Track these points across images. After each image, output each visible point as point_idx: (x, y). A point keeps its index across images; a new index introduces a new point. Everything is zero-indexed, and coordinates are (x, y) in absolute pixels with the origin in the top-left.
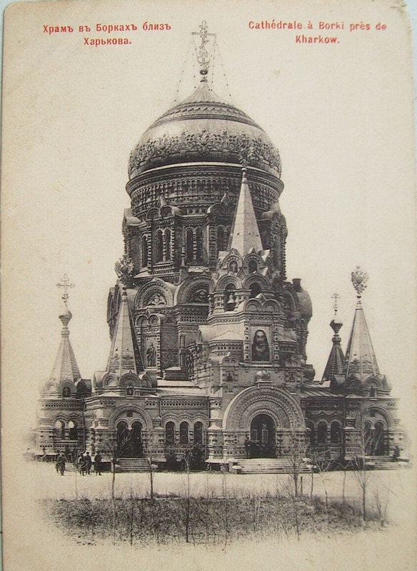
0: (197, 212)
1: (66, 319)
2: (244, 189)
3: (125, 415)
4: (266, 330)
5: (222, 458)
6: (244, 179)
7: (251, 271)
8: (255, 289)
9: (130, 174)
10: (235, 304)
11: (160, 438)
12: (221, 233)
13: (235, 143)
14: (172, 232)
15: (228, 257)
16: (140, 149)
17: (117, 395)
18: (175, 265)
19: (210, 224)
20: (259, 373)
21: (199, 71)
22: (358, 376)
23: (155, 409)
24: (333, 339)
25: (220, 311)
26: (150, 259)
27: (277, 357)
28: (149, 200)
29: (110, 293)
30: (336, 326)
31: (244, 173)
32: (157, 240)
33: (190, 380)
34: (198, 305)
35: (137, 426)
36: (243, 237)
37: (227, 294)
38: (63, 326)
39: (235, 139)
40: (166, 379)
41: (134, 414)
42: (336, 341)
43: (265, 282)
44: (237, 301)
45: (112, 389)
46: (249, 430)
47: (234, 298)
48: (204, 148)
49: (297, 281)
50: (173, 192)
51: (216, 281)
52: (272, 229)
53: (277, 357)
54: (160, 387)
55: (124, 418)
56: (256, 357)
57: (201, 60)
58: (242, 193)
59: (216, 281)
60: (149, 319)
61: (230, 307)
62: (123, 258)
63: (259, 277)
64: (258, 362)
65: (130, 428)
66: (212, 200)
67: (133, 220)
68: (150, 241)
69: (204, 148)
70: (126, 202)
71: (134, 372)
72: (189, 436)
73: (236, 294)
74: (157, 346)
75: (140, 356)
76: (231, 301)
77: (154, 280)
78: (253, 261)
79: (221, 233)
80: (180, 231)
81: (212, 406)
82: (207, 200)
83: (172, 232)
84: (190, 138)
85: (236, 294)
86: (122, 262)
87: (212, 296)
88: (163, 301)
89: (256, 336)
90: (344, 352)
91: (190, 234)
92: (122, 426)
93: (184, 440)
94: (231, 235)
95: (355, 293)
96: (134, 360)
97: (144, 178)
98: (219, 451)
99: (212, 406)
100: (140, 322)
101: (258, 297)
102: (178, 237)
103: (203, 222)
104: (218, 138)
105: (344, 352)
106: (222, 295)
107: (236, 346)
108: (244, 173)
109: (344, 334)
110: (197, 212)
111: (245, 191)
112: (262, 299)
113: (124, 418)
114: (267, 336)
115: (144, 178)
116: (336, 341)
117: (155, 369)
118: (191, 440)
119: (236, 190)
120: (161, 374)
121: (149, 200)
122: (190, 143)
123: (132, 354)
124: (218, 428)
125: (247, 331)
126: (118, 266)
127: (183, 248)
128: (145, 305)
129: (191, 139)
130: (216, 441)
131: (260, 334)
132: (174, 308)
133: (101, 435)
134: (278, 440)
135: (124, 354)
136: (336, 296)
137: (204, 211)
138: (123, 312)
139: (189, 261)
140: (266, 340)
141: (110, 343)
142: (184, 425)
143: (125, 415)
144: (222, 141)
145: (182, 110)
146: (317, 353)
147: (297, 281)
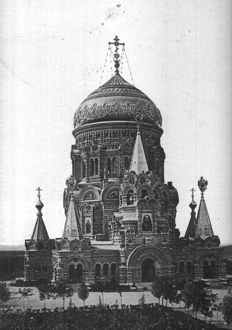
0: (87, 255)
2: (138, 137)
3: (73, 261)
4: (150, 215)
6: (138, 133)
7: (142, 183)
8: (144, 193)
9: (75, 125)
11: (92, 273)
12: (126, 158)
13: (134, 109)
14: (99, 159)
16: (79, 112)
17: (69, 251)
18: (101, 178)
19: (120, 155)
20: (147, 238)
22: (202, 237)
23: (89, 257)
24: (191, 213)
25: (125, 205)
26: (87, 171)
27: (156, 229)
29: (65, 192)
30: (193, 206)
31: (138, 129)
32: (90, 163)
33: (110, 241)
34: (112, 199)
35: (80, 266)
36: (138, 163)
38: (39, 212)
39: (134, 107)
40: (96, 240)
41: (78, 261)
43: (149, 188)
44: (134, 199)
46: (141, 267)
47: (133, 198)
48: (116, 113)
49: (170, 183)
51: (123, 189)
52: (156, 157)
53: (156, 229)
54: (92, 245)
55: (73, 263)
56: (144, 229)
58: (137, 140)
59: (123, 189)
62: (70, 177)
63: (147, 186)
64: (146, 232)
65: (76, 268)
66: (121, 141)
68: (86, 164)
69: (116, 113)
71: (78, 238)
72: (109, 271)
73: (134, 196)
74: (91, 222)
75: (83, 228)
77: (89, 186)
78: (142, 178)
79: (126, 158)
80: (104, 159)
81: (121, 255)
82: (119, 141)
83: (99, 159)
84: (109, 107)
85: (134, 196)
86: (70, 179)
87: (121, 196)
89: (144, 218)
91: (109, 159)
93: (106, 273)
94: (131, 163)
96: (77, 232)
97: (82, 129)
98: (126, 280)
99: (121, 255)
100: (82, 209)
101: (145, 198)
102: (102, 162)
103: (116, 153)
104: (124, 107)
106: (126, 196)
107: (134, 223)
108: (138, 129)
110: (113, 148)
112: (148, 198)
113: (73, 263)
114: (151, 218)
115: (82, 129)
116: (193, 214)
117: (91, 234)
118: (110, 273)
119: (134, 136)
120: (94, 237)
121: (86, 141)
122: (108, 110)
123: (76, 229)
124: (124, 267)
125: (140, 216)
126: (67, 181)
127: (105, 169)
128: (84, 200)
129: (109, 108)
131: (147, 217)
133: (59, 272)
134: (157, 273)
135: (72, 229)
137: (117, 148)
138: (72, 205)
139: (108, 176)
140: (150, 220)
141: (65, 218)
142: (106, 266)
143: (73, 261)
144: (127, 109)
145: (104, 90)
146: (182, 223)
147: (170, 183)
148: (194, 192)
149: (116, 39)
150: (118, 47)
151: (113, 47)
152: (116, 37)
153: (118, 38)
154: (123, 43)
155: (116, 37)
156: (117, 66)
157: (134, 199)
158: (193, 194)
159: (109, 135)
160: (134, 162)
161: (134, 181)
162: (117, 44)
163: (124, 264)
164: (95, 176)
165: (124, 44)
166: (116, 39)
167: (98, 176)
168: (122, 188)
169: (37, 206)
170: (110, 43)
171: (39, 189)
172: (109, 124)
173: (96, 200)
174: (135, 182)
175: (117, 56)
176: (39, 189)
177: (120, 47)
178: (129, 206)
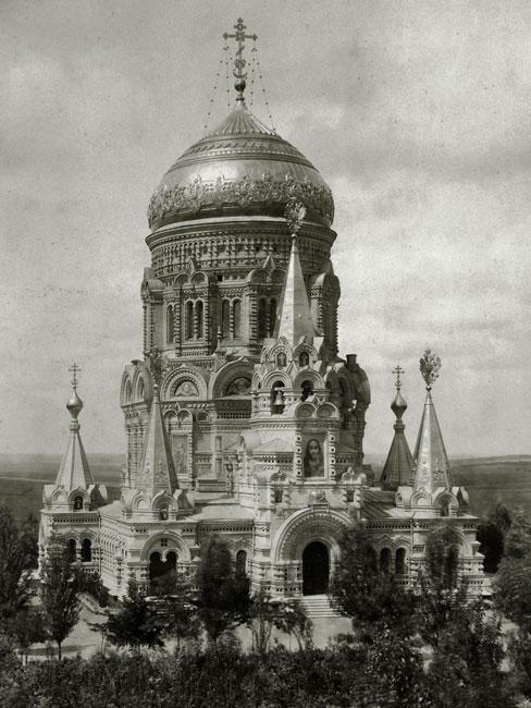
1: (75, 409)
5: (233, 497)
10: (283, 406)
15: (276, 347)
21: (223, 32)
28: (176, 261)
30: (398, 409)
37: (274, 395)
41: (169, 543)
42: (399, 429)
45: (143, 513)
49: (351, 358)
50: (205, 252)
57: (237, 72)
60: (179, 416)
61: (278, 410)
67: (155, 283)
70: (146, 258)
76: (278, 402)
77: (184, 365)
88: (195, 391)
90: (412, 451)
92: (155, 556)
95: (424, 384)
105: (412, 451)
109: (411, 420)
111: (295, 268)
112: (315, 402)
116: (399, 429)
128: (226, 395)
130: (263, 575)
132: (208, 402)
136: (398, 370)
147: (351, 358)
148: (401, 375)
149: (240, 25)
150: (243, 43)
151: (234, 44)
152: (240, 20)
153: (244, 24)
154: (252, 34)
155: (240, 20)
156: (75, 383)
157: (286, 403)
158: (398, 382)
159: (227, 249)
160: (284, 316)
161: (285, 360)
162: (240, 37)
163: (266, 552)
164: (194, 341)
165: (255, 38)
166: (240, 25)
167: (203, 341)
168: (260, 375)
169: (69, 407)
170: (226, 36)
171: (75, 369)
172: (201, 227)
173: (197, 399)
174: (288, 364)
175: (240, 64)
176: (75, 369)
177: (248, 43)
178: (274, 416)
